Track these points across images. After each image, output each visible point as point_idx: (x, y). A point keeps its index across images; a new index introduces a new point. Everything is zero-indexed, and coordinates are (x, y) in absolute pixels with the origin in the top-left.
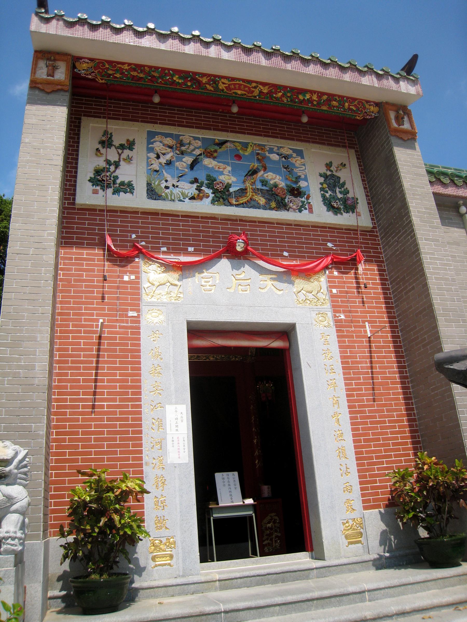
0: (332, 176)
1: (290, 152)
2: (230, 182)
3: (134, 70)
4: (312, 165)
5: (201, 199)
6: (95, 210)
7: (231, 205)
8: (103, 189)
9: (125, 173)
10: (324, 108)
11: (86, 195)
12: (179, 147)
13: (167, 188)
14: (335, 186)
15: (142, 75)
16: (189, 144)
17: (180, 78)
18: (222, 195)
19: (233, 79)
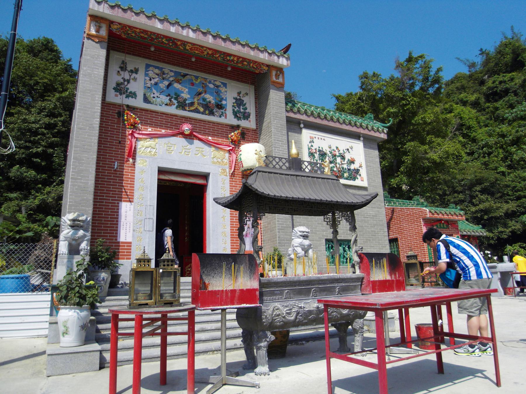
0: (240, 99)
1: (219, 84)
2: (187, 97)
3: (142, 33)
4: (230, 93)
5: (171, 105)
6: (116, 105)
7: (186, 110)
8: (121, 94)
9: (132, 87)
10: (240, 65)
11: (113, 98)
12: (162, 75)
13: (154, 97)
14: (240, 105)
15: (146, 36)
16: (168, 74)
17: (166, 40)
18: (182, 105)
19: (194, 44)
